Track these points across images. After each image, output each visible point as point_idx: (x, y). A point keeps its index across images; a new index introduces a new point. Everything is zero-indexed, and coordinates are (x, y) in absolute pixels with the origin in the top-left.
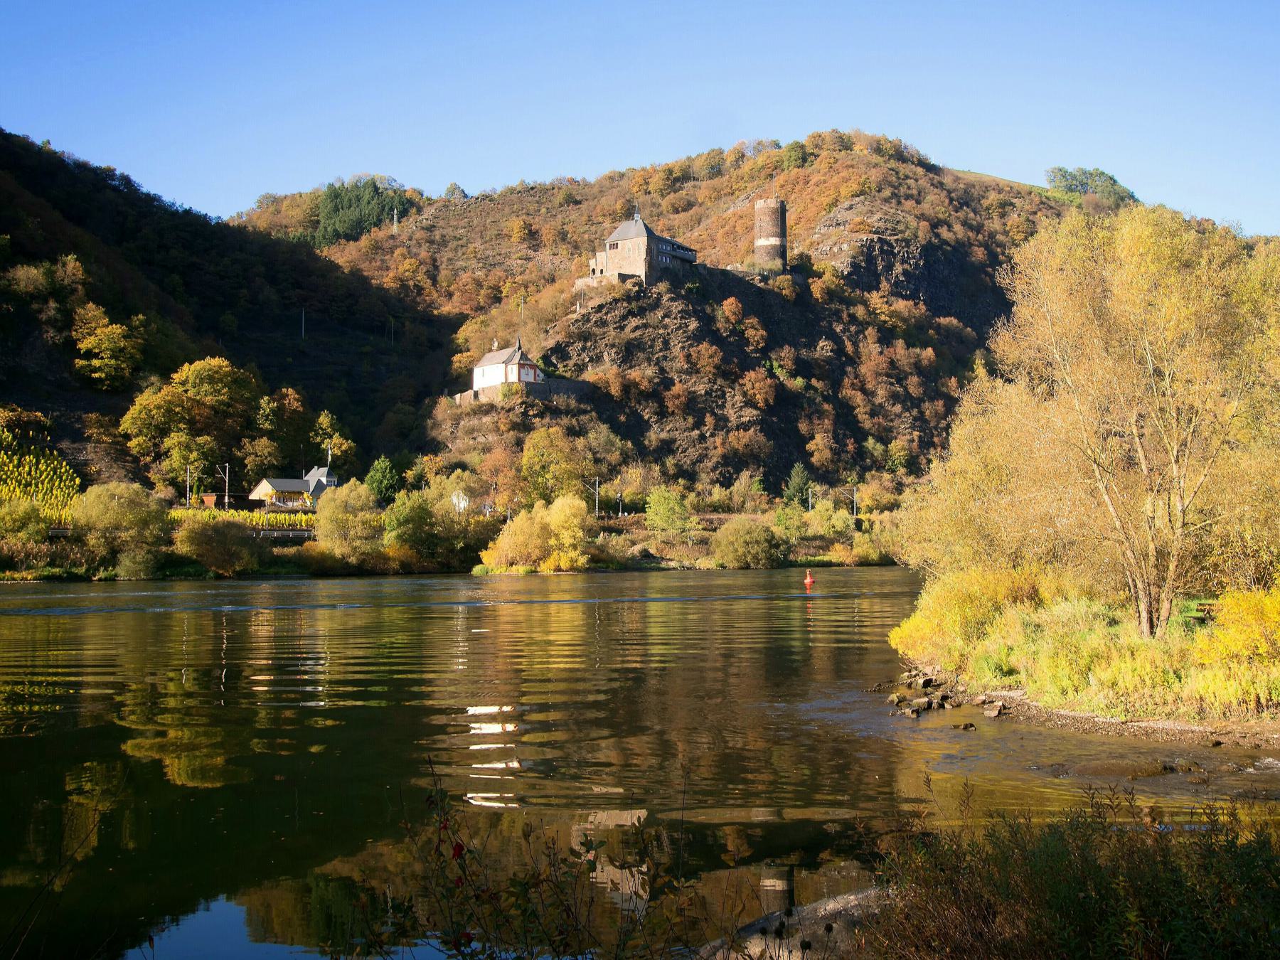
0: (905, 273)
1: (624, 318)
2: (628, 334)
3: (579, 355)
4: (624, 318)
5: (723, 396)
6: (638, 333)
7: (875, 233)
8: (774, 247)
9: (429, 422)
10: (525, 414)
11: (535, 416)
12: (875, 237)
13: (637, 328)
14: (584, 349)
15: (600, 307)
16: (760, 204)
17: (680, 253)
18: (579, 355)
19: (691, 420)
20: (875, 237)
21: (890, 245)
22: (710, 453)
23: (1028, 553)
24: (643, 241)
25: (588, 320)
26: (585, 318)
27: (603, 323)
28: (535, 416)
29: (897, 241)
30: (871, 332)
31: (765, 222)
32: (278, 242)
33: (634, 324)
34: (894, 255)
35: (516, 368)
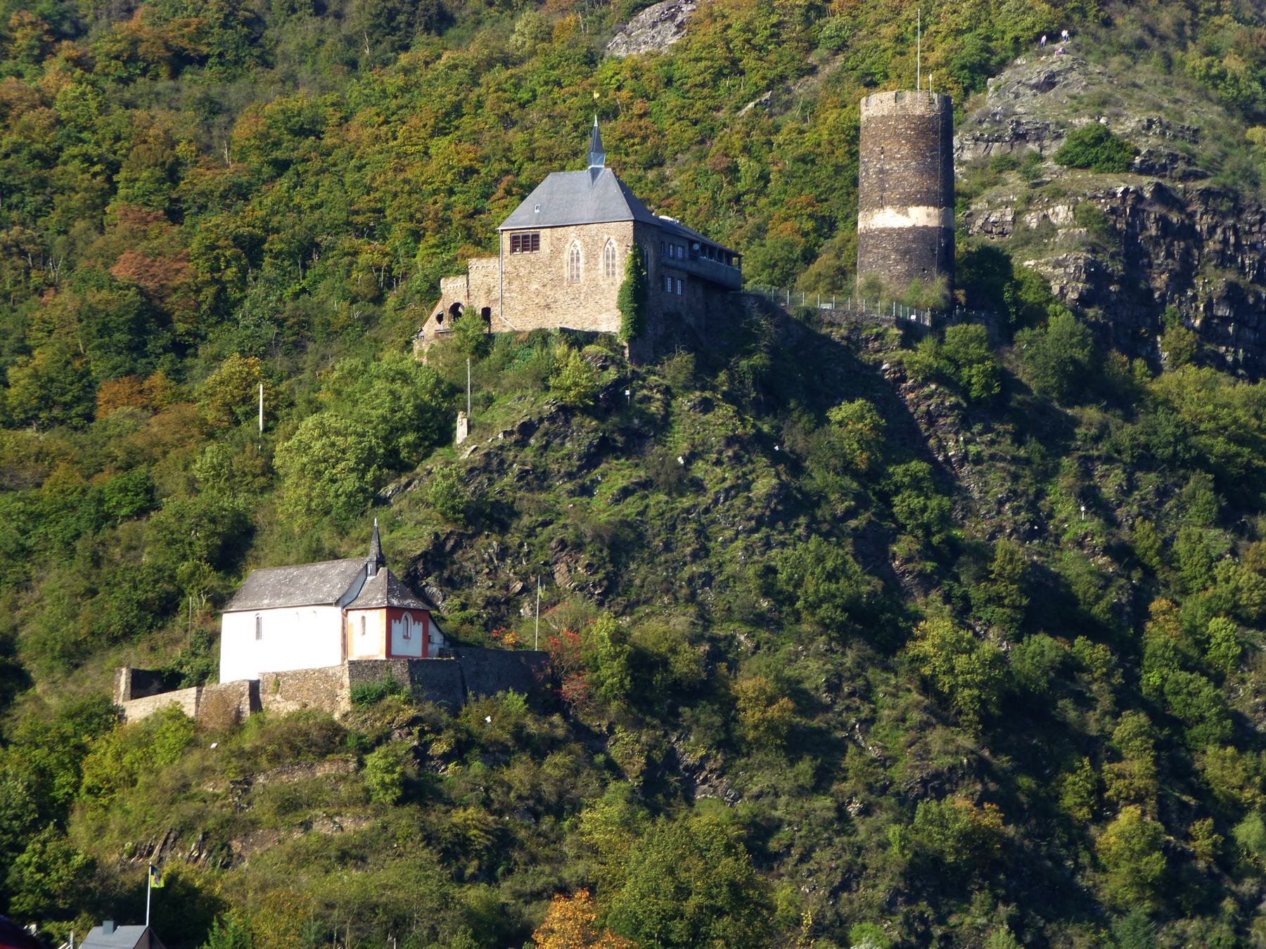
0: (1233, 294)
1: (592, 459)
2: (602, 509)
3: (493, 573)
4: (592, 459)
5: (866, 693)
6: (630, 508)
7: (1145, 170)
8: (921, 234)
9: (470, 931)
10: (421, 753)
11: (446, 758)
12: (1147, 184)
13: (626, 492)
14: (503, 553)
15: (527, 429)
16: (876, 105)
17: (707, 265)
18: (493, 573)
19: (806, 766)
20: (1147, 184)
21: (1180, 205)
22: (873, 860)
24: (617, 239)
25: (502, 469)
26: (492, 464)
27: (537, 479)
28: (446, 758)
29: (1206, 194)
30: (1198, 487)
31: (888, 159)
33: (622, 483)
34: (1198, 240)
35: (377, 620)
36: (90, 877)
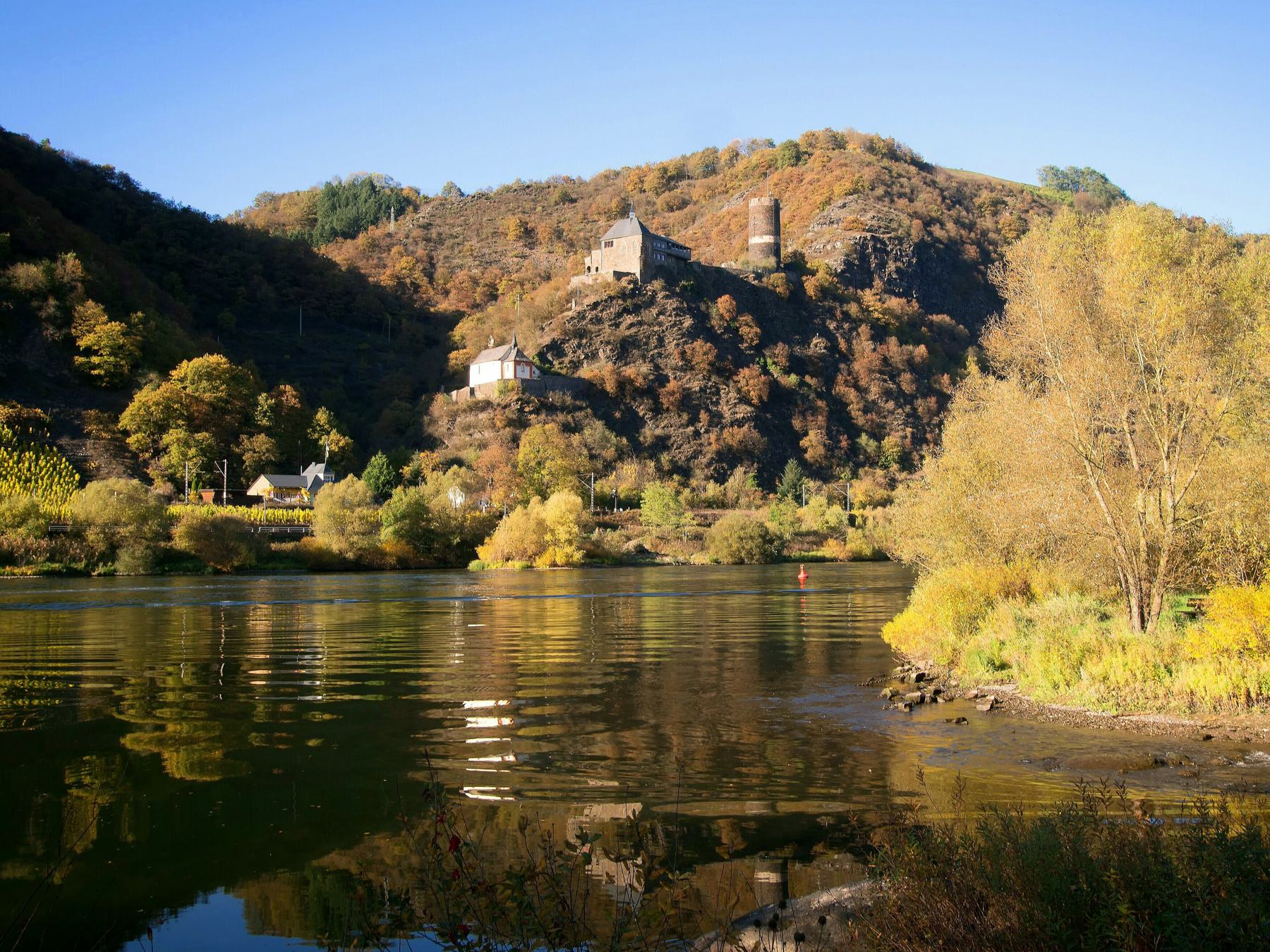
0: (898, 270)
1: (619, 315)
2: (623, 331)
3: (574, 352)
4: (619, 315)
5: (718, 392)
6: (633, 330)
7: (868, 231)
8: (768, 245)
9: (426, 419)
10: (521, 410)
11: (531, 413)
12: (869, 235)
13: (632, 325)
14: (579, 346)
15: (596, 305)
16: (754, 202)
17: (675, 251)
18: (574, 352)
19: (685, 416)
20: (869, 235)
21: (883, 243)
22: (705, 450)
23: (1020, 549)
24: (638, 239)
25: (584, 318)
26: (581, 315)
27: (599, 321)
28: (531, 413)
29: (890, 239)
30: (864, 329)
31: (759, 220)
32: (276, 240)
33: (629, 322)
34: (887, 253)
35: (512, 365)
36: (998, 911)
